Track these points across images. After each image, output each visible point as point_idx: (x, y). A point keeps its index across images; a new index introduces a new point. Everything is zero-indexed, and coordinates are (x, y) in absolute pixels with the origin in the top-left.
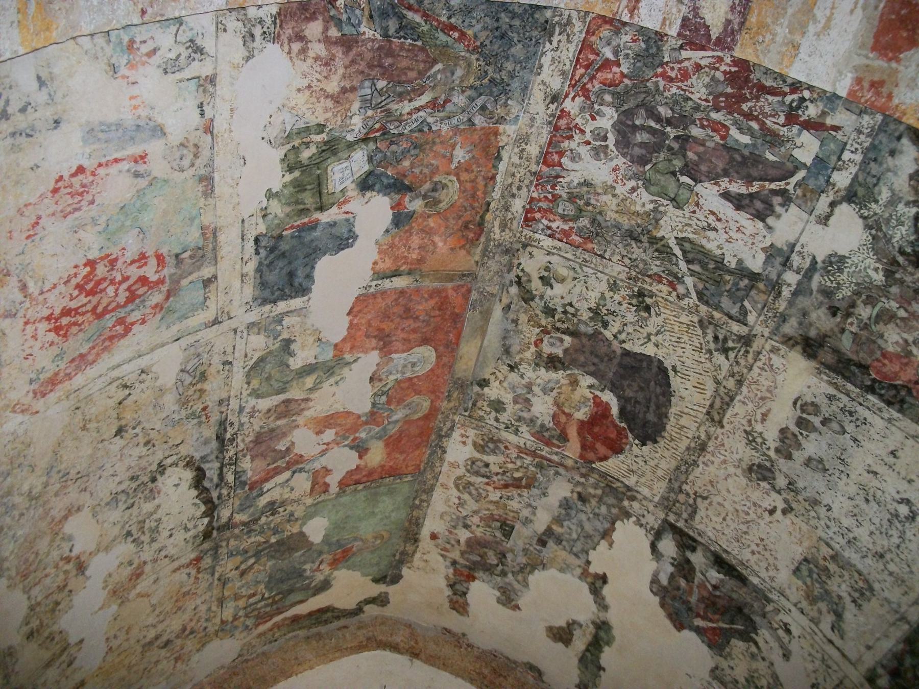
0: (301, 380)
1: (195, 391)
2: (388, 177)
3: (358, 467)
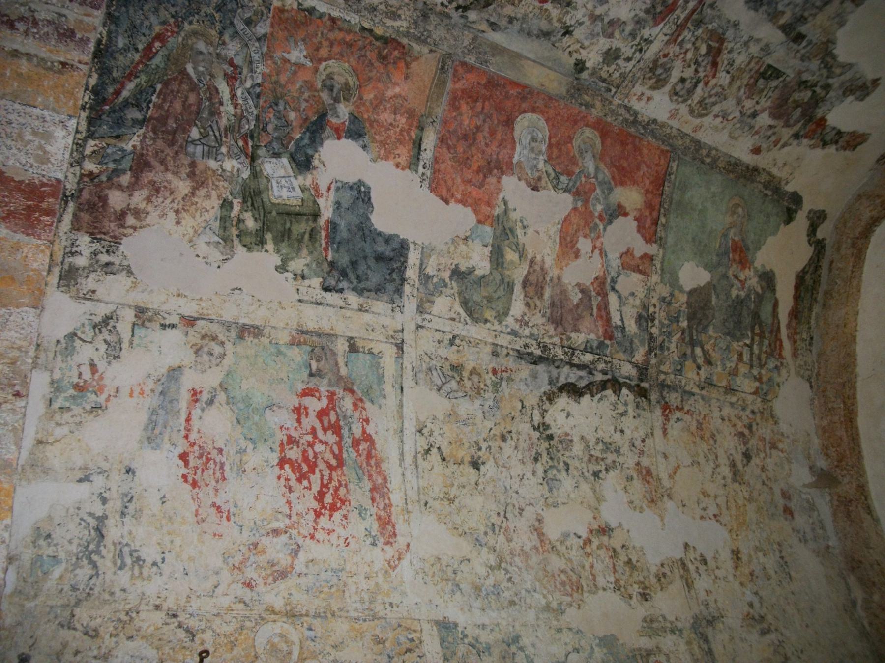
2: (302, 139)
3: (636, 219)
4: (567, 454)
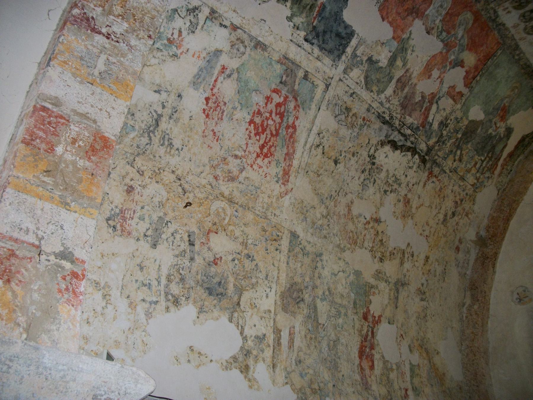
0: (394, 66)
1: (351, 118)
4: (377, 176)
